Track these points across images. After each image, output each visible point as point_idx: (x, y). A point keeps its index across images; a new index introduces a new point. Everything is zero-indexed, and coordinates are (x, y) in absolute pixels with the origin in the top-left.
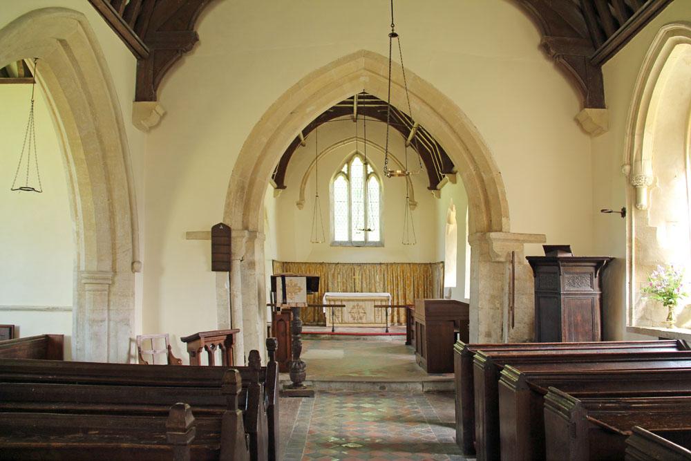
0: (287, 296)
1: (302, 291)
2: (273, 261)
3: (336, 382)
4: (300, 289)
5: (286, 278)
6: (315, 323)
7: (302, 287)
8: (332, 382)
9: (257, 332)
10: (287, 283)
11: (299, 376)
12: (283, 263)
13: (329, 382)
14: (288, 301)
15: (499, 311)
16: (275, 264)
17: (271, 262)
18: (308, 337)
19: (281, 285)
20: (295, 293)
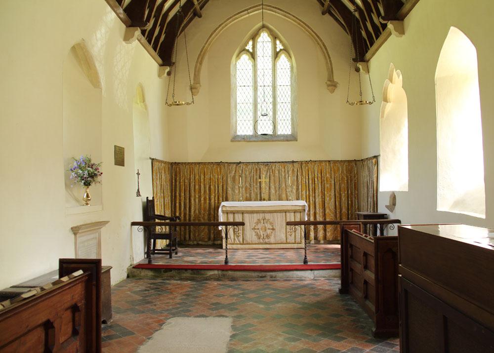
16: (156, 164)
17: (150, 161)
18: (187, 274)
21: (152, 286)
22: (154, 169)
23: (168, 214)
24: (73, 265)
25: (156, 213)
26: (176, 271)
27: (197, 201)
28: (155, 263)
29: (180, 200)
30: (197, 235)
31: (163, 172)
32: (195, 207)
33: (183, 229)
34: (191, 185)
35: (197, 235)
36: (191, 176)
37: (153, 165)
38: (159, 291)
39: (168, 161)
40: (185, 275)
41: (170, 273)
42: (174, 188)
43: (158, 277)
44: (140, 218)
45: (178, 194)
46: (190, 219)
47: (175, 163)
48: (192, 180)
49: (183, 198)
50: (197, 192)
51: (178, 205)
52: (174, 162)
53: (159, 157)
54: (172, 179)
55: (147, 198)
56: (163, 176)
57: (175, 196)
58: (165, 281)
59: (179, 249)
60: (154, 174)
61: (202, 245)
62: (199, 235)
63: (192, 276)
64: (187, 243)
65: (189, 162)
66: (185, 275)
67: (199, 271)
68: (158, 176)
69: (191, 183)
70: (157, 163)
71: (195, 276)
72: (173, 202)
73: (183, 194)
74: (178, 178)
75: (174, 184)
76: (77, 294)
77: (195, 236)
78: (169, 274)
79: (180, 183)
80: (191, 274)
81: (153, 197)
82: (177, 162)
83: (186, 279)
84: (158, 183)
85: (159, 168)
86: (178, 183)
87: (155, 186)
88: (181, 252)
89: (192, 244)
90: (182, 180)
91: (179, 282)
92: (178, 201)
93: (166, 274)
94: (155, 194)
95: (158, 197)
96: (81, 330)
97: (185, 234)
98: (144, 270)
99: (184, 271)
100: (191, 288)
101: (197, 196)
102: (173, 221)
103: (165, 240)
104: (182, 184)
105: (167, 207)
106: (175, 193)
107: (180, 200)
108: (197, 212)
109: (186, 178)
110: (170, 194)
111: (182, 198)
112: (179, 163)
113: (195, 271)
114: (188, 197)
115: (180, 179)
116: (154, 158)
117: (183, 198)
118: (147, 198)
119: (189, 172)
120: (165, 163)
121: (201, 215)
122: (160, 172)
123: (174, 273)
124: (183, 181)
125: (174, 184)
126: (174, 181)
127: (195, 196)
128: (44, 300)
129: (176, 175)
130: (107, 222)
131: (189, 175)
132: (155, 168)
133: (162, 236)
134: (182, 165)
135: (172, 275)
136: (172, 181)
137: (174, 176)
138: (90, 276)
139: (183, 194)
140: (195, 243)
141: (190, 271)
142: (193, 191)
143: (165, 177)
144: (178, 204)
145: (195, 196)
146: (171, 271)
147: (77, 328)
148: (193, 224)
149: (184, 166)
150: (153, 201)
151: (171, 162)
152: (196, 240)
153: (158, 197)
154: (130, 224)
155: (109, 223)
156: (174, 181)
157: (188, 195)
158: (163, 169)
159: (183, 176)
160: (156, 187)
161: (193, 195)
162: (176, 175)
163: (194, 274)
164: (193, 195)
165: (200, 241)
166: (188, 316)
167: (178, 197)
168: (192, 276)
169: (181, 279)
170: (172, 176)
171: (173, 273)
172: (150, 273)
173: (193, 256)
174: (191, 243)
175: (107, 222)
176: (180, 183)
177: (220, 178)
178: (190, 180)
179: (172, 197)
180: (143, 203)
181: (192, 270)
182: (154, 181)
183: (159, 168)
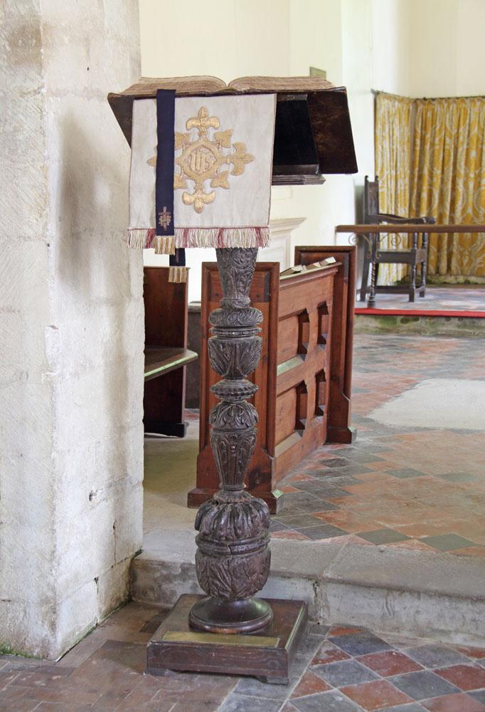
0: (178, 194)
1: (249, 168)
2: (377, 94)
3: (416, 593)
4: (242, 159)
5: (179, 103)
6: (451, 279)
7: (252, 149)
8: (401, 590)
9: (47, 367)
10: (180, 128)
11: (233, 572)
12: (416, 101)
13: (389, 589)
14: (180, 222)
15: (246, 232)
16: (384, 104)
17: (371, 97)
18: (452, 326)
19: (154, 141)
20: (219, 180)
21: (380, 342)
22: (378, 116)
23: (403, 212)
24: (315, 255)
25: (381, 211)
26: (428, 320)
27: (471, 185)
28: (379, 306)
29: (431, 185)
30: (465, 261)
31: (397, 121)
32: (465, 199)
33: (435, 250)
34: (460, 150)
35: (465, 261)
36: (461, 130)
37: (378, 106)
38: (398, 349)
39: (407, 96)
40: (445, 328)
41: (415, 323)
42: (417, 159)
43: (388, 331)
44: (350, 220)
45: (426, 172)
46: (452, 219)
47: (425, 99)
48: (461, 139)
49: (437, 181)
50: (473, 167)
51: (425, 195)
52: (421, 96)
53: (389, 87)
54: (415, 137)
55: (366, 177)
56: (395, 132)
57: (420, 177)
58: (403, 338)
59: (427, 290)
60: (379, 126)
61: (476, 283)
62: (471, 261)
63: (460, 330)
64: (442, 279)
65: (459, 95)
66: (445, 328)
67: (476, 321)
68: (387, 130)
69: (460, 144)
70: (386, 101)
71: (467, 330)
72: (415, 191)
73: (438, 172)
74: (428, 136)
75: (418, 148)
76: (323, 291)
77: (462, 265)
78: (412, 325)
79: (433, 144)
80: (459, 326)
81: (376, 177)
82: (428, 96)
83: (448, 335)
84: (386, 145)
85: (389, 112)
86: (428, 147)
87: (380, 154)
88: (429, 293)
89: (454, 282)
90: (437, 140)
91: (434, 339)
92: (425, 188)
93: (407, 325)
94: (379, 169)
95: (385, 176)
96: (328, 338)
97: (439, 259)
98: (361, 317)
99: (443, 320)
100: (458, 347)
101: (472, 175)
102: (414, 225)
103: (395, 265)
104: (437, 147)
105: (401, 199)
106: (421, 169)
107: (431, 185)
108: (470, 211)
109: (448, 134)
110: (408, 172)
111: (435, 179)
112: (433, 100)
113: (467, 321)
114: (451, 179)
115: (433, 137)
116: (380, 90)
117: (437, 181)
118: (366, 177)
119: (455, 120)
120: (401, 100)
121: (478, 217)
122: (391, 120)
123: (423, 325)
124: (440, 140)
125: (418, 148)
126: (418, 142)
127: (467, 176)
128: (300, 284)
129: (424, 128)
130: (302, 220)
131: (455, 128)
132: (380, 115)
133: (392, 257)
134: (440, 103)
135: (418, 328)
136: (415, 142)
137: (419, 130)
138: (340, 268)
139: (438, 172)
140: (461, 279)
141: (456, 321)
142: (463, 163)
143: (400, 132)
144: (425, 195)
145: (467, 176)
146: (417, 320)
147: (323, 335)
148: (462, 230)
149: (446, 105)
150: (376, 184)
151: (414, 96)
152: (462, 274)
153: (385, 176)
154: (333, 229)
155: (302, 225)
156: (418, 142)
157: (451, 174)
158: (398, 115)
159: (440, 129)
160: (382, 156)
161: (462, 172)
162: (424, 128)
163: (465, 326)
164: (462, 172)
165: (472, 275)
166: (459, 378)
167: (426, 177)
168: (460, 330)
169: (437, 335)
170: (415, 131)
171: (421, 323)
172: (374, 323)
173: (460, 300)
174: (451, 279)
175: (302, 220)
176: (433, 144)
177: (439, 151)
178: (458, 138)
179: (412, 179)
180: (357, 188)
181: (461, 317)
182: (378, 142)
183: (389, 112)
